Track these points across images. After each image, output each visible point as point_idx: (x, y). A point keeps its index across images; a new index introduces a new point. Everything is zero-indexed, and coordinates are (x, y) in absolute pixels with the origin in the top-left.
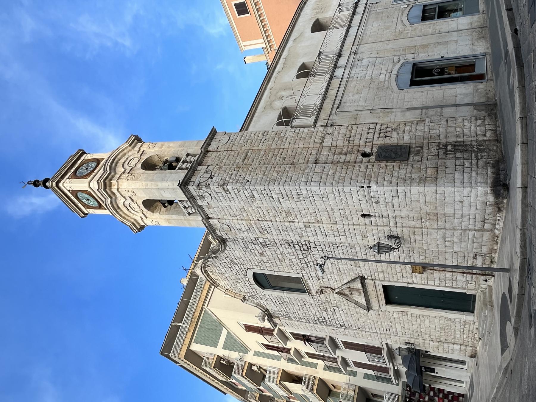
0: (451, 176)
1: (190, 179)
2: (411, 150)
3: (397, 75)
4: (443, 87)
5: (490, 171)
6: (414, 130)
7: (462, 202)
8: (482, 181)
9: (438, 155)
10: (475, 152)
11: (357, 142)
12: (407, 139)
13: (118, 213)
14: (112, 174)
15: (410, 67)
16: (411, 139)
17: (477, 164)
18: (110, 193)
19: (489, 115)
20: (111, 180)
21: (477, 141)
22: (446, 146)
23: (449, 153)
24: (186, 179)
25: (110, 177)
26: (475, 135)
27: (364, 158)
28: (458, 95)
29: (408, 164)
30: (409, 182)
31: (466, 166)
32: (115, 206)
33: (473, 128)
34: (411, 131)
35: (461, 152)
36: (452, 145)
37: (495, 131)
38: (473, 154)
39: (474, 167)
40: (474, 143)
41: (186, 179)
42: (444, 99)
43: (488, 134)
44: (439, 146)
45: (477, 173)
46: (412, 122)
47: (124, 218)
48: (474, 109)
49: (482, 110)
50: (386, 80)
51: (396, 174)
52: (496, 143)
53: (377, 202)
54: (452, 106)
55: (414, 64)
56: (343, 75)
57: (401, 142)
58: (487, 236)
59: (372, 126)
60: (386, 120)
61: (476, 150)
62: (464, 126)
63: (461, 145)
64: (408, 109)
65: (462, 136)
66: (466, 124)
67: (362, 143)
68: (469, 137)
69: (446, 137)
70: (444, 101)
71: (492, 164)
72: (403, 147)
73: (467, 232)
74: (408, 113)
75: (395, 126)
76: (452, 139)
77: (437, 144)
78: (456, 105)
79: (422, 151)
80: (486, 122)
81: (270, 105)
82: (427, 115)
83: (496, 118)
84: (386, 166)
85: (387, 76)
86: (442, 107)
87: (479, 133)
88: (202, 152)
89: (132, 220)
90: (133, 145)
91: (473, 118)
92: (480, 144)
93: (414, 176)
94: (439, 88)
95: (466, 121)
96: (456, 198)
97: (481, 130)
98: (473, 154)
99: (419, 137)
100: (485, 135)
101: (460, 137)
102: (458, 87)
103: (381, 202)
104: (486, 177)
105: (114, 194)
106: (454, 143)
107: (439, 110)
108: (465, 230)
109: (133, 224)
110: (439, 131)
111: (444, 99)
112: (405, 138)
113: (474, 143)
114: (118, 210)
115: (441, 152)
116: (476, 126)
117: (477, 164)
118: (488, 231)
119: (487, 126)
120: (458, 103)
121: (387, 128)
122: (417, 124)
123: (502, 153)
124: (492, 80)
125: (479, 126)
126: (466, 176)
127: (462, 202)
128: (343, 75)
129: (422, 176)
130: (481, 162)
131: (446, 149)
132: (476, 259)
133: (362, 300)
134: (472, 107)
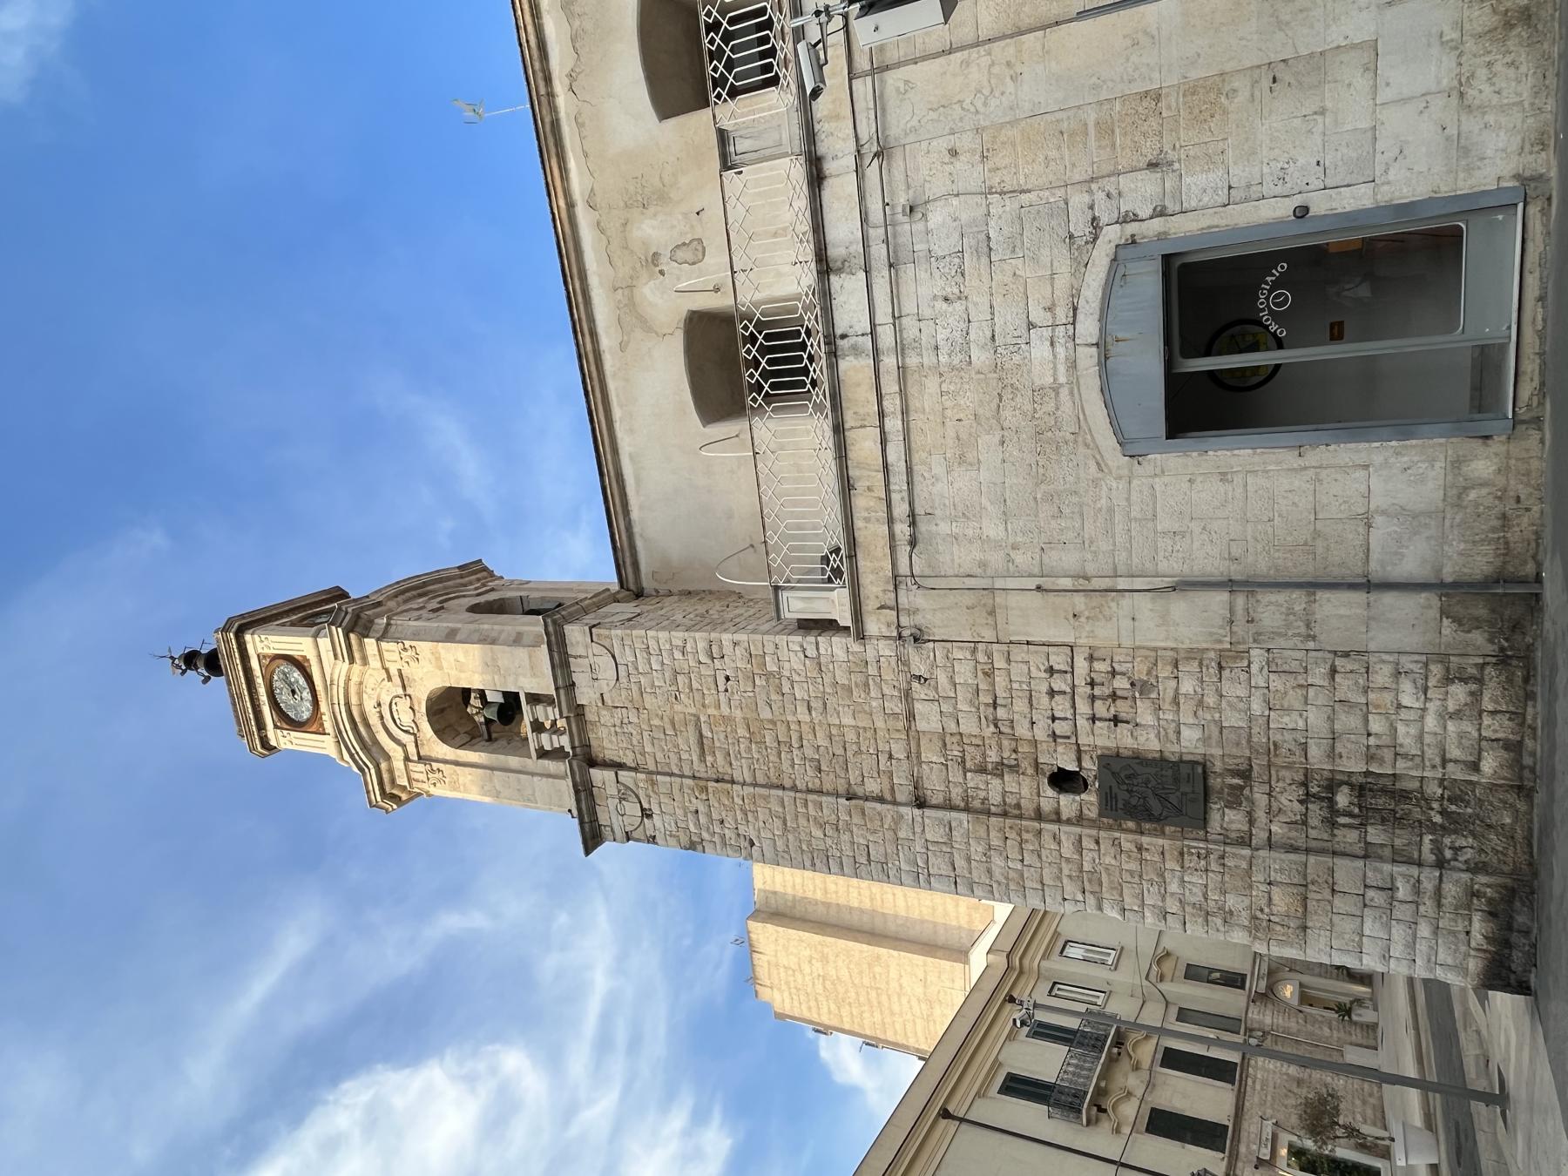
0: (1348, 926)
1: (594, 819)
2: (1211, 781)
3: (1102, 346)
4: (1315, 456)
5: (1479, 927)
6: (1211, 700)
8: (1450, 961)
9: (1305, 823)
10: (1433, 827)
11: (1022, 730)
12: (1190, 742)
14: (384, 766)
15: (1148, 285)
16: (1205, 740)
17: (1438, 894)
19: (1503, 660)
20: (393, 781)
21: (1441, 782)
22: (1332, 786)
23: (1342, 820)
24: (587, 826)
25: (386, 776)
26: (1438, 761)
28: (1379, 520)
29: (1209, 853)
30: (1219, 921)
31: (1401, 894)
33: (1431, 722)
34: (1200, 703)
35: (1383, 821)
36: (1351, 785)
37: (1513, 747)
38: (1427, 838)
39: (1428, 907)
40: (1434, 790)
41: (587, 826)
42: (1317, 534)
43: (1489, 765)
44: (1305, 784)
45: (1436, 930)
46: (1195, 655)
48: (1444, 613)
49: (1476, 623)
50: (1062, 379)
51: (1174, 887)
52: (1511, 797)
54: (1352, 586)
55: (1167, 259)
56: (873, 325)
57: (1172, 750)
59: (1059, 660)
60: (1103, 634)
61: (1438, 819)
62: (1399, 706)
63: (1384, 791)
64: (1184, 586)
65: (1388, 755)
66: (1406, 700)
67: (1041, 733)
68: (1416, 767)
69: (1332, 754)
70: (1320, 543)
71: (1490, 901)
72: (1185, 770)
74: (1179, 606)
75: (1140, 671)
76: (1353, 765)
77: (1300, 777)
78: (1369, 585)
79: (1246, 792)
80: (1486, 698)
81: (633, 315)
82: (1252, 628)
83: (1526, 680)
84: (1140, 848)
85: (1060, 350)
86: (1312, 586)
87: (1454, 752)
88: (567, 718)
90: (357, 655)
91: (1436, 670)
92: (1456, 793)
93: (1232, 901)
94: (1289, 458)
95: (1406, 686)
97: (1461, 735)
98: (1427, 838)
99: (1233, 736)
100: (1475, 767)
101: (1382, 761)
102: (1378, 459)
104: (1463, 948)
106: (1362, 780)
107: (1298, 599)
110: (1305, 720)
111: (1317, 534)
112: (1185, 732)
113: (1434, 790)
115: (1316, 811)
116: (1445, 716)
117: (1438, 894)
119: (1487, 720)
120: (1376, 570)
121: (1114, 673)
122: (1221, 668)
123: (1530, 845)
124: (1537, 422)
125: (1457, 715)
126: (1399, 932)
128: (873, 325)
129: (1258, 914)
130: (1451, 890)
131: (1331, 802)
134: (1430, 600)
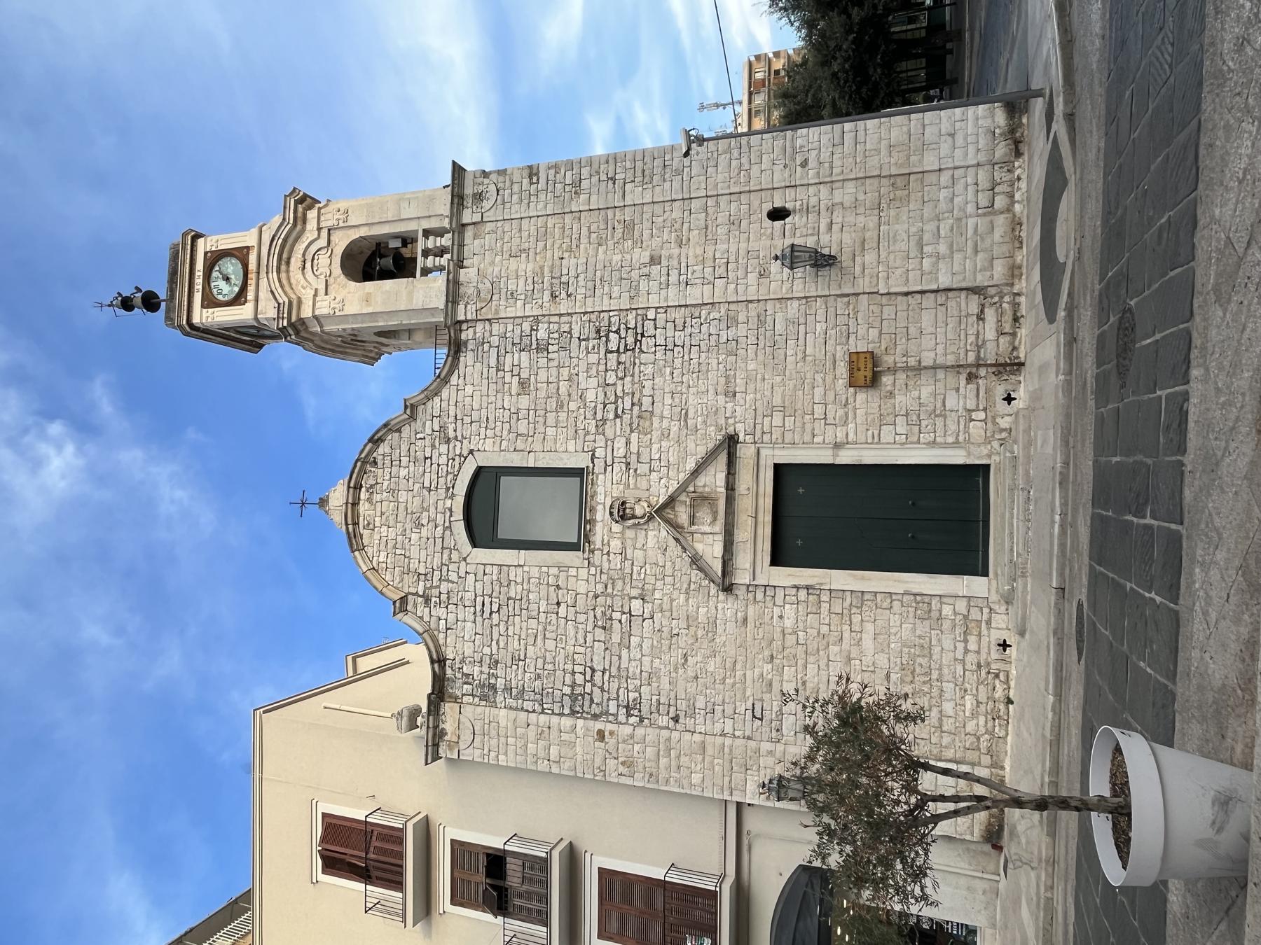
7: (952, 135)
13: (279, 272)
18: (300, 215)
27: (776, 223)
32: (285, 256)
47: (282, 286)
53: (804, 164)
58: (1001, 221)
73: (964, 221)
89: (293, 296)
96: (943, 127)
103: (810, 165)
105: (304, 221)
108: (959, 219)
109: (290, 303)
114: (283, 268)
118: (1002, 213)
120: (933, 295)
127: (952, 135)
132: (983, 320)
133: (712, 550)
